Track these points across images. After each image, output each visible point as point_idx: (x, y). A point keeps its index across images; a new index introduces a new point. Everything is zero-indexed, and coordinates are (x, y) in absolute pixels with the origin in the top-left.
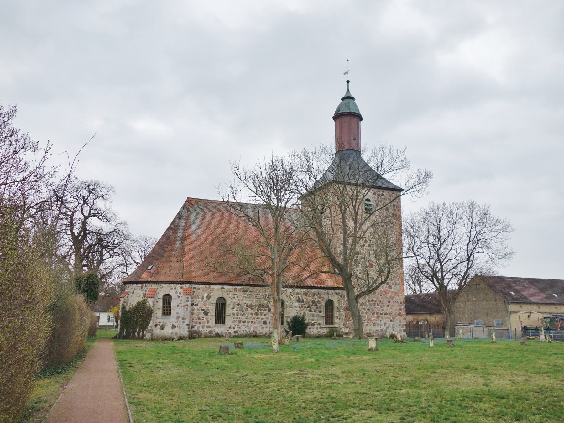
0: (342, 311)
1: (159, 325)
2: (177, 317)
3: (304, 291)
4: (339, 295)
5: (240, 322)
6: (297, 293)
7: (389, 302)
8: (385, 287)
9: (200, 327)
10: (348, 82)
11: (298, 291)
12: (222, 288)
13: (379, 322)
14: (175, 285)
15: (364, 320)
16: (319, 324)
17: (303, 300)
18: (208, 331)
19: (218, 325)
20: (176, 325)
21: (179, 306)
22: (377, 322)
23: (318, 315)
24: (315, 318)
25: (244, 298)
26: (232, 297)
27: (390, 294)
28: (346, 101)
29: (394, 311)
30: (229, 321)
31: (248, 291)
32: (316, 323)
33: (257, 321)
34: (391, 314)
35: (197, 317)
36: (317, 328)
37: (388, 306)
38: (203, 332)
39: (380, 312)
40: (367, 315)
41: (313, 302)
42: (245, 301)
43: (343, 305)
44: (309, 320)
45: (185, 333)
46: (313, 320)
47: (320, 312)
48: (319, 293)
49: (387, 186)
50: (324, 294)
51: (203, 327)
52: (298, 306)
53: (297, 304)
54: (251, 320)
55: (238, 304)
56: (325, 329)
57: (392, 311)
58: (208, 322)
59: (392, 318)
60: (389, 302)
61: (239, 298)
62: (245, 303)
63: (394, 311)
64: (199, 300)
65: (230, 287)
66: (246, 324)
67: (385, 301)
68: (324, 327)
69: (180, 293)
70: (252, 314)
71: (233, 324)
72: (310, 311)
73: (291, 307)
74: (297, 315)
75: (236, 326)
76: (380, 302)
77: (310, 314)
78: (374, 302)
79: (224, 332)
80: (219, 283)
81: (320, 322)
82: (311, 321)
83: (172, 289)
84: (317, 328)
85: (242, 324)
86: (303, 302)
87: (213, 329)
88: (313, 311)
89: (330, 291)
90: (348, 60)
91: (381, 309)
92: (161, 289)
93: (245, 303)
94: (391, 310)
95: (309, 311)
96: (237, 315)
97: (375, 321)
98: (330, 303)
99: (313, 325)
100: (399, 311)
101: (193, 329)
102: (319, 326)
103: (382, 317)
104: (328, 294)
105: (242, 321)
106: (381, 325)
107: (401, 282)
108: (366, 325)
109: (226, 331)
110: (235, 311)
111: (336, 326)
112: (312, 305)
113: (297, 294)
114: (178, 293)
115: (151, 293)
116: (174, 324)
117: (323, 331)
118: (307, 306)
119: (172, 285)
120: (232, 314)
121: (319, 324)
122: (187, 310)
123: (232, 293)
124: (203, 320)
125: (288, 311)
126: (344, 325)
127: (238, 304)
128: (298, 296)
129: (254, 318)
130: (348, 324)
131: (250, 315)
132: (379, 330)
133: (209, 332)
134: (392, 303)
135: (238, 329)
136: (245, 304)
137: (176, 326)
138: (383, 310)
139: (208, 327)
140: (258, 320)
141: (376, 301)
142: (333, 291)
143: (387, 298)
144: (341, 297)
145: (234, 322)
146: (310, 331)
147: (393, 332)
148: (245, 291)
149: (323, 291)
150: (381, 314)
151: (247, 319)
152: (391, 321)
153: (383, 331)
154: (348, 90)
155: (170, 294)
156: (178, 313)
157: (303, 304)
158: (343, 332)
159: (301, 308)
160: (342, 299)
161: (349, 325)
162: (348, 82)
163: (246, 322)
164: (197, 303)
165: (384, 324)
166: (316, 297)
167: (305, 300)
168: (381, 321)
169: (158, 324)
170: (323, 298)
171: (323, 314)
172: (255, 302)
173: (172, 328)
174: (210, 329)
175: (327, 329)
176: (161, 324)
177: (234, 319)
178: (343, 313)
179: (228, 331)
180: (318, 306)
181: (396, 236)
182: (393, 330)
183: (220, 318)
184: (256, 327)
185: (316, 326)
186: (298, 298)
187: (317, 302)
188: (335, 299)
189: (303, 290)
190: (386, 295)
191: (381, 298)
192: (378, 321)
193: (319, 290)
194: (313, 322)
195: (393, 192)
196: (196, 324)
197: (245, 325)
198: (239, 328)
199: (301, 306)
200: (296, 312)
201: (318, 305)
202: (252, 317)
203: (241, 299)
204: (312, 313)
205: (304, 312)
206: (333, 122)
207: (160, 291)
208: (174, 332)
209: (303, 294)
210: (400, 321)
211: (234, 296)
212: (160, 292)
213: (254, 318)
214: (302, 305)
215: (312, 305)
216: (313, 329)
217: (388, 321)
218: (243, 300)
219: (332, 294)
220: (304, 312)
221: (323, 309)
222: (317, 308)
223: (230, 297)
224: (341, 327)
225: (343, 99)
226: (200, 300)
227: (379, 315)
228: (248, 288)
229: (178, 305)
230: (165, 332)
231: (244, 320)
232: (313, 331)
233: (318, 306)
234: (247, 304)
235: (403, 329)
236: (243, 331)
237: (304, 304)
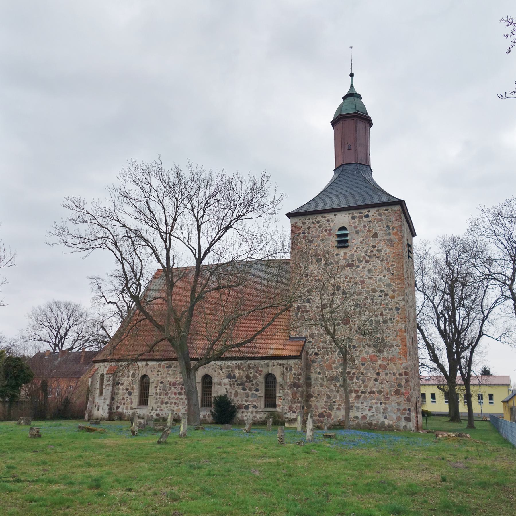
0: (288, 389)
3: (236, 364)
4: (283, 367)
5: (162, 403)
6: (228, 367)
7: (378, 374)
8: (370, 352)
9: (124, 408)
10: (352, 75)
11: (229, 364)
12: (147, 365)
13: (360, 405)
15: (334, 402)
16: (255, 407)
17: (234, 375)
18: (131, 413)
19: (141, 407)
22: (356, 404)
23: (253, 394)
24: (250, 399)
25: (168, 375)
26: (155, 374)
27: (380, 362)
28: (349, 99)
29: (386, 387)
30: (151, 402)
31: (173, 367)
32: (250, 406)
33: (180, 402)
34: (382, 392)
35: (122, 397)
36: (252, 413)
37: (376, 380)
38: (127, 414)
39: (363, 389)
40: (338, 394)
41: (248, 377)
42: (168, 379)
43: (288, 380)
44: (242, 401)
45: (106, 415)
46: (247, 401)
47: (257, 390)
48: (255, 365)
49: (387, 199)
50: (262, 366)
51: (127, 409)
52: (229, 383)
53: (227, 381)
54: (173, 401)
55: (162, 383)
56: (263, 413)
57: (382, 388)
58: (132, 403)
59: (382, 398)
60: (378, 374)
61: (163, 375)
62: (169, 381)
63: (386, 387)
64: (124, 378)
65: (154, 363)
66: (168, 405)
67: (371, 374)
68: (261, 410)
70: (175, 394)
71: (155, 405)
72: (244, 389)
73: (220, 385)
74: (226, 395)
75: (158, 407)
76: (362, 374)
77: (244, 393)
78: (351, 375)
79: (146, 415)
80: (168, 359)
81: (256, 404)
82: (244, 403)
84: (252, 413)
85: (164, 405)
86: (234, 377)
87: (135, 411)
88: (247, 389)
89: (271, 362)
90: (351, 48)
91: (363, 385)
93: (169, 381)
94: (381, 386)
95: (242, 390)
96: (160, 395)
97: (353, 403)
98: (270, 379)
99: (247, 407)
100: (397, 388)
101: (118, 410)
102: (254, 410)
103: (365, 397)
104: (268, 366)
105: (164, 402)
106: (364, 410)
107: (400, 342)
108: (338, 409)
109: (148, 414)
110: (158, 391)
111: (278, 409)
112: (246, 382)
113: (227, 368)
117: (260, 416)
118: (239, 383)
120: (154, 394)
121: (255, 407)
122: (108, 390)
123: (156, 370)
124: (127, 400)
125: (216, 390)
126: (290, 408)
127: (162, 383)
128: (228, 370)
129: (177, 399)
130: (295, 407)
131: (173, 395)
132: (360, 417)
133: (132, 414)
134: (382, 376)
135: (160, 411)
136: (169, 382)
138: (366, 386)
139: (132, 408)
140: (182, 401)
141: (354, 374)
142: (276, 362)
143: (374, 368)
144: (286, 369)
145: (156, 403)
146: (242, 416)
147: (385, 420)
148: (169, 367)
149: (262, 362)
150: (362, 392)
151: (170, 399)
152: (381, 403)
153: (366, 418)
154: (352, 86)
157: (234, 380)
158: (288, 418)
159: (232, 386)
160: (287, 373)
161: (297, 408)
162: (352, 75)
163: (169, 403)
164: (122, 382)
165: (367, 408)
166: (252, 371)
167: (237, 375)
168: (362, 403)
170: (261, 371)
171: (261, 393)
172: (179, 379)
174: (133, 411)
175: (265, 413)
177: (156, 399)
178: (289, 392)
179: (150, 413)
180: (254, 382)
181: (392, 272)
182: (386, 418)
183: (144, 400)
184: (179, 409)
185: (250, 409)
186: (228, 373)
187: (253, 377)
188: (277, 372)
189: (234, 362)
190: (373, 363)
191: (364, 368)
192: (358, 403)
193: (256, 362)
194: (247, 404)
195: (385, 208)
196: (121, 405)
197: (167, 407)
198: (162, 410)
199: (232, 383)
200: (226, 390)
201: (254, 381)
202: (175, 398)
203: (165, 376)
204: (246, 392)
205: (236, 391)
206: (331, 131)
209: (234, 367)
210: (399, 404)
211: (158, 373)
213: (177, 399)
214: (233, 381)
215: (246, 382)
216: (247, 413)
217: (376, 403)
218: (166, 377)
219: (274, 366)
220: (236, 391)
221: (262, 387)
222: (253, 385)
223: (153, 375)
224: (286, 411)
225: (344, 98)
226: (126, 378)
227: (359, 394)
228: (172, 363)
231: (166, 401)
232: (246, 416)
233: (254, 382)
234: (171, 382)
235: (405, 416)
236: (166, 413)
237: (236, 381)
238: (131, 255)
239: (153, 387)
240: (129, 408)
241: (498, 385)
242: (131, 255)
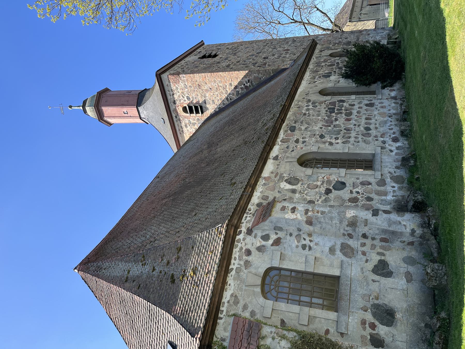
1: (373, 326)
2: (345, 254)
14: (236, 253)
20: (375, 259)
21: (307, 242)
55: (322, 136)
69: (266, 238)
83: (247, 264)
92: (241, 305)
114: (264, 243)
115: (118, 110)
116: (370, 266)
119: (235, 264)
133: (396, 182)
137: (379, 258)
139: (382, 183)
155: (262, 271)
156: (332, 250)
169: (369, 330)
173: (389, 274)
174: (388, 180)
176: (369, 317)
207: (245, 307)
208: (404, 268)
212: (250, 309)
229: (304, 247)
230: (405, 306)
238: (304, 24)
239: (330, 147)
240: (382, 188)
241: (255, 285)
242: (304, 24)
